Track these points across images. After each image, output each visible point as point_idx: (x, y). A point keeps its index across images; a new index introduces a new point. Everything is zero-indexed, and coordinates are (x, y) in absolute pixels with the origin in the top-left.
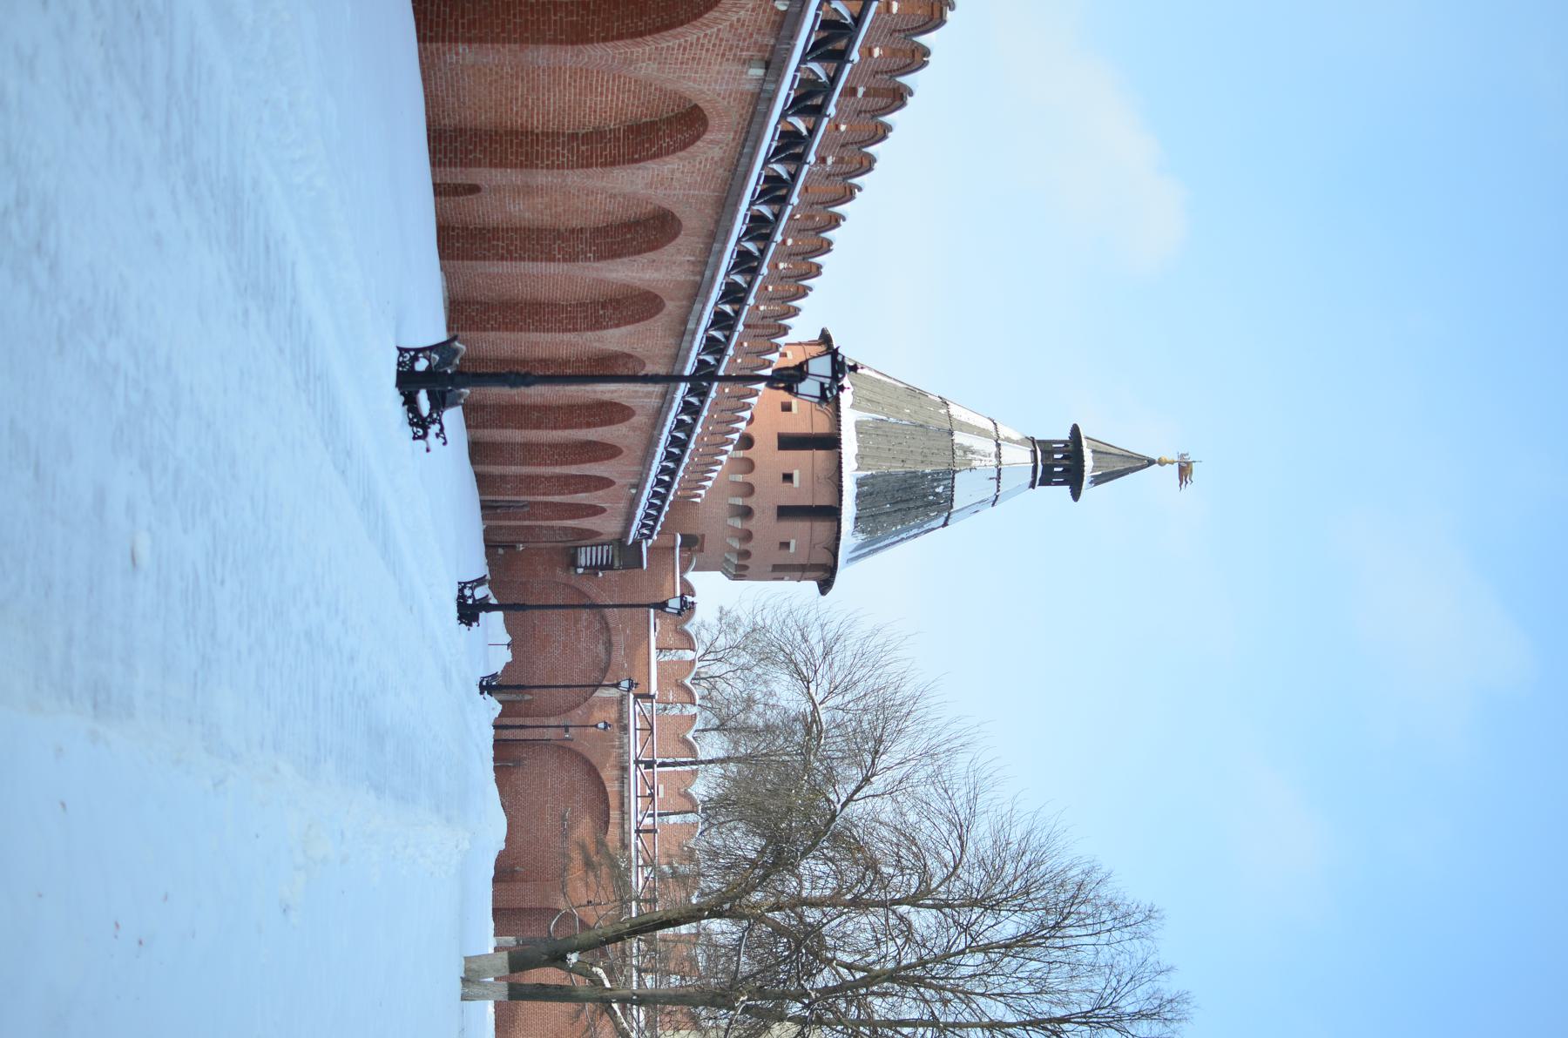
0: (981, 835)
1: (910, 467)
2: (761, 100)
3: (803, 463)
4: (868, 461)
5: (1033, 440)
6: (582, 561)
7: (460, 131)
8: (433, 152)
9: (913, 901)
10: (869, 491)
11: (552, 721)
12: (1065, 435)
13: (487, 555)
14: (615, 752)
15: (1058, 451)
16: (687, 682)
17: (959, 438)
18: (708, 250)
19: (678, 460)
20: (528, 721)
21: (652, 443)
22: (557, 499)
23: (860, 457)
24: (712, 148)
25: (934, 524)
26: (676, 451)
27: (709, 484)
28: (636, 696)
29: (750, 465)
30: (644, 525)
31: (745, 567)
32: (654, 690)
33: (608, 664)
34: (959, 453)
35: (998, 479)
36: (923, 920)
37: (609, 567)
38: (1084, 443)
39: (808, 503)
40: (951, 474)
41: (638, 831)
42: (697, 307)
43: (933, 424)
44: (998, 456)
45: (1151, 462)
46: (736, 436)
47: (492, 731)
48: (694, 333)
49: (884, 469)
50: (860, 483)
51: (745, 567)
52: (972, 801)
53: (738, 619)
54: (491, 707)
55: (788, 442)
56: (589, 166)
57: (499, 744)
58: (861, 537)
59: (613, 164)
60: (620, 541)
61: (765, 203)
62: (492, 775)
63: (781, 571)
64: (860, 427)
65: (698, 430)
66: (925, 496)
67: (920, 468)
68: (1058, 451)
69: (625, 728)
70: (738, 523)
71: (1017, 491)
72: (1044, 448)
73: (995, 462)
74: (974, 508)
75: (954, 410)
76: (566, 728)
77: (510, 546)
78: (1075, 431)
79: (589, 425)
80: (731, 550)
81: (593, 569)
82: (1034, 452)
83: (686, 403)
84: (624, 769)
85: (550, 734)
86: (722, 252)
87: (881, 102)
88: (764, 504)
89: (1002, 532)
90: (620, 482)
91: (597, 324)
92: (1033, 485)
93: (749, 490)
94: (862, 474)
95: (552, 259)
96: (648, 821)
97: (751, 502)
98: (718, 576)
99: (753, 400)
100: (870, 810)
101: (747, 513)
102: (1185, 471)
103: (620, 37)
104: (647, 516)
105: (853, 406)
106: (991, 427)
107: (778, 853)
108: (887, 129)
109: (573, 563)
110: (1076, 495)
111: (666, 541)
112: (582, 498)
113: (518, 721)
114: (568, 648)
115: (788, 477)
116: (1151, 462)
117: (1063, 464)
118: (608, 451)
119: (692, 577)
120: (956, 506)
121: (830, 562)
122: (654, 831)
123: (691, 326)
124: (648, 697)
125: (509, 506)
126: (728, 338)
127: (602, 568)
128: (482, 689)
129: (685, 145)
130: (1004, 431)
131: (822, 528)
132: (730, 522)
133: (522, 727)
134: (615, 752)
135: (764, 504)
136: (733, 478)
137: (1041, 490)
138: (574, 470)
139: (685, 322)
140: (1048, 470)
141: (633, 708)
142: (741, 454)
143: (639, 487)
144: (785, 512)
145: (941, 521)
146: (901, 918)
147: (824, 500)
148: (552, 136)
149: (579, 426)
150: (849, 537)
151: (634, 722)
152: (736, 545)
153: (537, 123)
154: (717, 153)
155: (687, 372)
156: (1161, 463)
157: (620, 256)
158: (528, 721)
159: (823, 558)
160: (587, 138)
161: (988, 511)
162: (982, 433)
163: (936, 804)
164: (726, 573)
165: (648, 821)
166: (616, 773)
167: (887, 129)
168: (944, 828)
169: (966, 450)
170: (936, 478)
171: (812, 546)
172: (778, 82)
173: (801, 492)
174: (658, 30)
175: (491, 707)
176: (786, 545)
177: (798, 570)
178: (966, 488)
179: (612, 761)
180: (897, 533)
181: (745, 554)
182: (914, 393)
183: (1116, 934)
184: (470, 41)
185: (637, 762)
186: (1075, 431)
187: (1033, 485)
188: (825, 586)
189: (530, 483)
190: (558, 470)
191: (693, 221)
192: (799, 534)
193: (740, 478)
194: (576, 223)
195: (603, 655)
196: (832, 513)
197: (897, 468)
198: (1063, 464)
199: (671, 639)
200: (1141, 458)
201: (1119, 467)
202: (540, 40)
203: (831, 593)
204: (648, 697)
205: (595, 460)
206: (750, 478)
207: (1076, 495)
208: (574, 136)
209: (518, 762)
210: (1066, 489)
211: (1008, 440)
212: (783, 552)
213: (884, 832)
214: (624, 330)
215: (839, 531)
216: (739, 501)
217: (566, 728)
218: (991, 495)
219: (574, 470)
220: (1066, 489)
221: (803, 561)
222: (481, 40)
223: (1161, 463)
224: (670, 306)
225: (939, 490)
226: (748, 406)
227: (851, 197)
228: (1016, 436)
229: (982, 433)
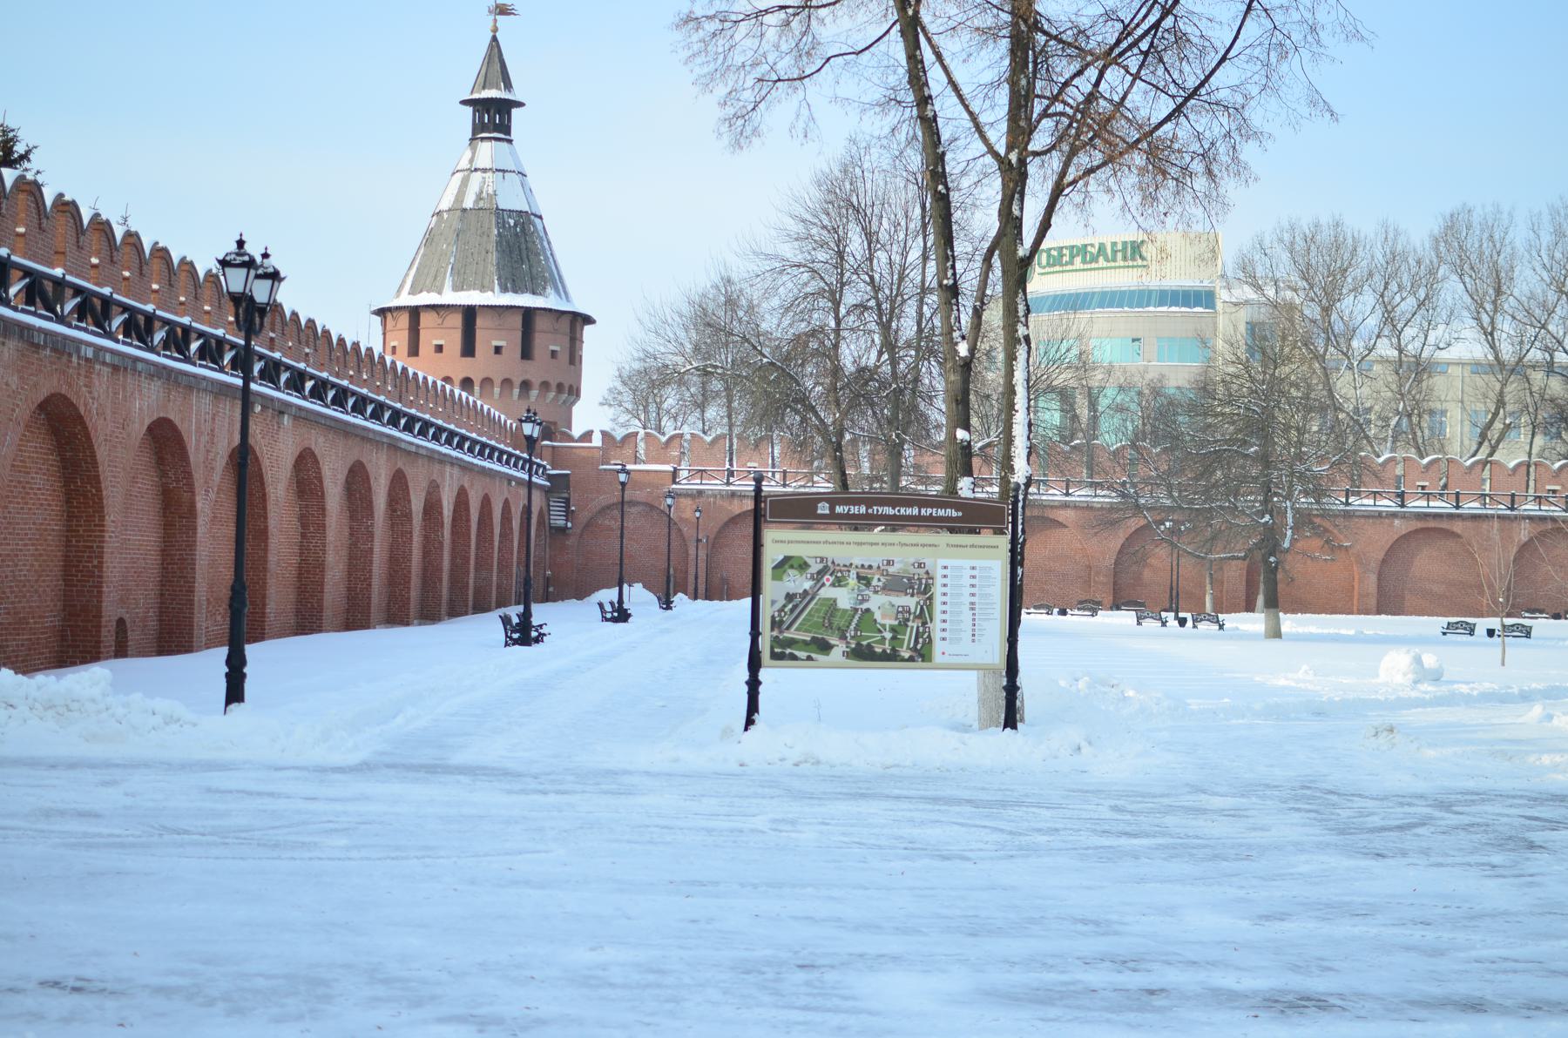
0: (790, 251)
1: (492, 247)
2: (302, 416)
3: (486, 338)
4: (486, 282)
5: (472, 140)
6: (561, 523)
7: (298, 612)
8: (312, 631)
9: (837, 304)
10: (512, 283)
11: (692, 551)
12: (469, 110)
13: (555, 601)
14: (719, 502)
15: (482, 118)
16: (664, 439)
17: (469, 203)
18: (369, 440)
19: (427, 424)
20: (692, 571)
21: (484, 471)
22: (496, 544)
23: (483, 289)
24: (320, 443)
25: (540, 227)
26: (417, 427)
27: (503, 417)
28: (674, 482)
29: (487, 381)
30: (507, 463)
31: (571, 387)
32: (669, 468)
33: (646, 504)
34: (481, 204)
35: (504, 171)
36: (850, 298)
37: (567, 501)
38: (476, 96)
39: (519, 334)
40: (499, 212)
41: (784, 485)
42: (403, 445)
43: (457, 225)
44: (485, 170)
45: (494, 39)
46: (464, 395)
47: (699, 601)
48: (418, 446)
49: (493, 269)
50: (504, 289)
51: (571, 387)
52: (768, 257)
53: (610, 390)
54: (680, 599)
55: (468, 349)
56: (324, 526)
57: (708, 597)
58: (549, 290)
59: (324, 509)
60: (547, 492)
61: (222, 358)
62: (734, 602)
63: (574, 358)
64: (457, 288)
65: (413, 411)
66: (516, 234)
67: (494, 238)
68: (482, 118)
69: (700, 492)
70: (534, 393)
71: (514, 154)
72: (478, 127)
73: (489, 174)
74: (528, 192)
75: (445, 205)
76: (698, 541)
77: (548, 581)
78: (464, 102)
79: (468, 520)
80: (555, 399)
81: (569, 514)
82: (482, 139)
83: (405, 429)
84: (733, 494)
85: (702, 554)
86: (374, 431)
87: (278, 319)
88: (517, 369)
89: (549, 170)
90: (506, 495)
91: (408, 516)
92: (510, 141)
93: (507, 382)
94: (497, 288)
95: (371, 549)
96: (778, 476)
97: (517, 381)
98: (576, 409)
99: (430, 380)
100: (775, 324)
101: (526, 386)
102: (503, 10)
103: (265, 508)
104: (471, 450)
105: (440, 293)
106: (459, 176)
107: (796, 401)
108: (183, 260)
109: (563, 530)
110: (520, 104)
111: (546, 453)
112: (516, 524)
113: (691, 579)
114: (644, 539)
115: (498, 350)
116: (494, 39)
117: (493, 116)
118: (486, 502)
119: (576, 432)
120: (526, 208)
121: (570, 317)
122: (785, 472)
123: (413, 449)
124: (675, 473)
125: (477, 591)
126: (334, 385)
127: (568, 506)
128: (669, 608)
129: (316, 462)
130: (464, 164)
131: (540, 323)
132: (533, 399)
133: (271, 795)
134: (719, 502)
135: (517, 369)
136: (496, 396)
137: (514, 135)
138: (497, 531)
139: (409, 453)
140: (497, 128)
141: (684, 485)
142: (477, 388)
143: (510, 478)
144: (526, 354)
145: (537, 221)
146: (848, 313)
147: (517, 321)
148: (303, 550)
149: (468, 528)
150: (547, 301)
151: (695, 485)
152: (552, 395)
153: (295, 560)
154: (321, 440)
155: (253, 386)
156: (495, 30)
157: (371, 502)
158: (692, 571)
159: (565, 324)
160: (304, 526)
161: (529, 179)
162: (465, 183)
163: (768, 283)
164: (573, 403)
165: (778, 476)
166: (736, 501)
167: (183, 260)
168: (785, 278)
169: (479, 198)
170: (502, 224)
171: (555, 331)
172: (289, 405)
173: (510, 340)
174: (263, 484)
175: (680, 599)
176: (554, 353)
177: (575, 342)
178: (512, 199)
179: (726, 504)
180: (546, 259)
181: (560, 387)
182: (430, 238)
183: (866, 166)
184: (264, 605)
185: (728, 483)
186: (464, 102)
187: (510, 141)
188: (588, 320)
189: (504, 566)
190: (496, 544)
191: (356, 452)
192: (545, 342)
193: (497, 390)
194: (346, 532)
195: (640, 508)
196: (528, 314)
197: (493, 257)
198: (493, 116)
199: (628, 451)
200: (491, 47)
201: (498, 67)
202: (264, 559)
203: (594, 317)
204: (675, 473)
205: (467, 510)
206: (497, 381)
207: (520, 104)
208: (303, 536)
209: (725, 581)
210: (515, 111)
211: (471, 161)
212: (559, 355)
213: (786, 322)
214: (413, 497)
215: (544, 309)
216: (516, 391)
217: (698, 541)
218: (517, 178)
219: (497, 531)
220: (515, 111)
221: (567, 339)
222: (264, 597)
223: (495, 30)
224: (400, 465)
225: (512, 222)
226: (434, 383)
227: (165, 251)
228: (468, 154)
229: (465, 183)
